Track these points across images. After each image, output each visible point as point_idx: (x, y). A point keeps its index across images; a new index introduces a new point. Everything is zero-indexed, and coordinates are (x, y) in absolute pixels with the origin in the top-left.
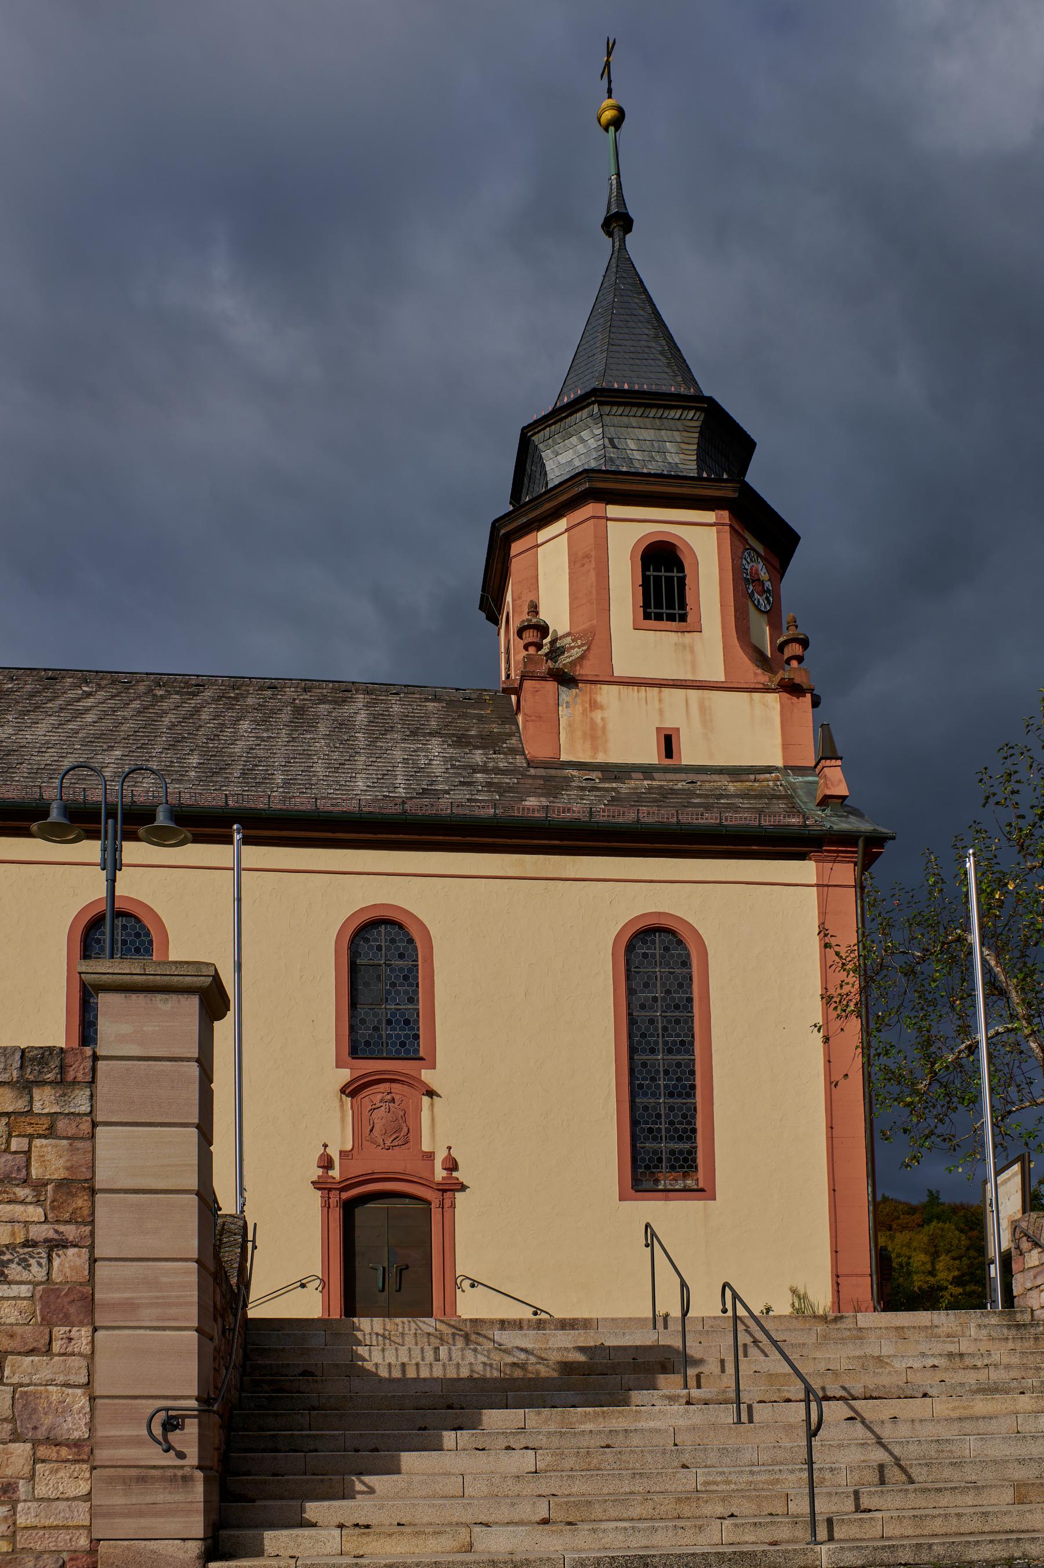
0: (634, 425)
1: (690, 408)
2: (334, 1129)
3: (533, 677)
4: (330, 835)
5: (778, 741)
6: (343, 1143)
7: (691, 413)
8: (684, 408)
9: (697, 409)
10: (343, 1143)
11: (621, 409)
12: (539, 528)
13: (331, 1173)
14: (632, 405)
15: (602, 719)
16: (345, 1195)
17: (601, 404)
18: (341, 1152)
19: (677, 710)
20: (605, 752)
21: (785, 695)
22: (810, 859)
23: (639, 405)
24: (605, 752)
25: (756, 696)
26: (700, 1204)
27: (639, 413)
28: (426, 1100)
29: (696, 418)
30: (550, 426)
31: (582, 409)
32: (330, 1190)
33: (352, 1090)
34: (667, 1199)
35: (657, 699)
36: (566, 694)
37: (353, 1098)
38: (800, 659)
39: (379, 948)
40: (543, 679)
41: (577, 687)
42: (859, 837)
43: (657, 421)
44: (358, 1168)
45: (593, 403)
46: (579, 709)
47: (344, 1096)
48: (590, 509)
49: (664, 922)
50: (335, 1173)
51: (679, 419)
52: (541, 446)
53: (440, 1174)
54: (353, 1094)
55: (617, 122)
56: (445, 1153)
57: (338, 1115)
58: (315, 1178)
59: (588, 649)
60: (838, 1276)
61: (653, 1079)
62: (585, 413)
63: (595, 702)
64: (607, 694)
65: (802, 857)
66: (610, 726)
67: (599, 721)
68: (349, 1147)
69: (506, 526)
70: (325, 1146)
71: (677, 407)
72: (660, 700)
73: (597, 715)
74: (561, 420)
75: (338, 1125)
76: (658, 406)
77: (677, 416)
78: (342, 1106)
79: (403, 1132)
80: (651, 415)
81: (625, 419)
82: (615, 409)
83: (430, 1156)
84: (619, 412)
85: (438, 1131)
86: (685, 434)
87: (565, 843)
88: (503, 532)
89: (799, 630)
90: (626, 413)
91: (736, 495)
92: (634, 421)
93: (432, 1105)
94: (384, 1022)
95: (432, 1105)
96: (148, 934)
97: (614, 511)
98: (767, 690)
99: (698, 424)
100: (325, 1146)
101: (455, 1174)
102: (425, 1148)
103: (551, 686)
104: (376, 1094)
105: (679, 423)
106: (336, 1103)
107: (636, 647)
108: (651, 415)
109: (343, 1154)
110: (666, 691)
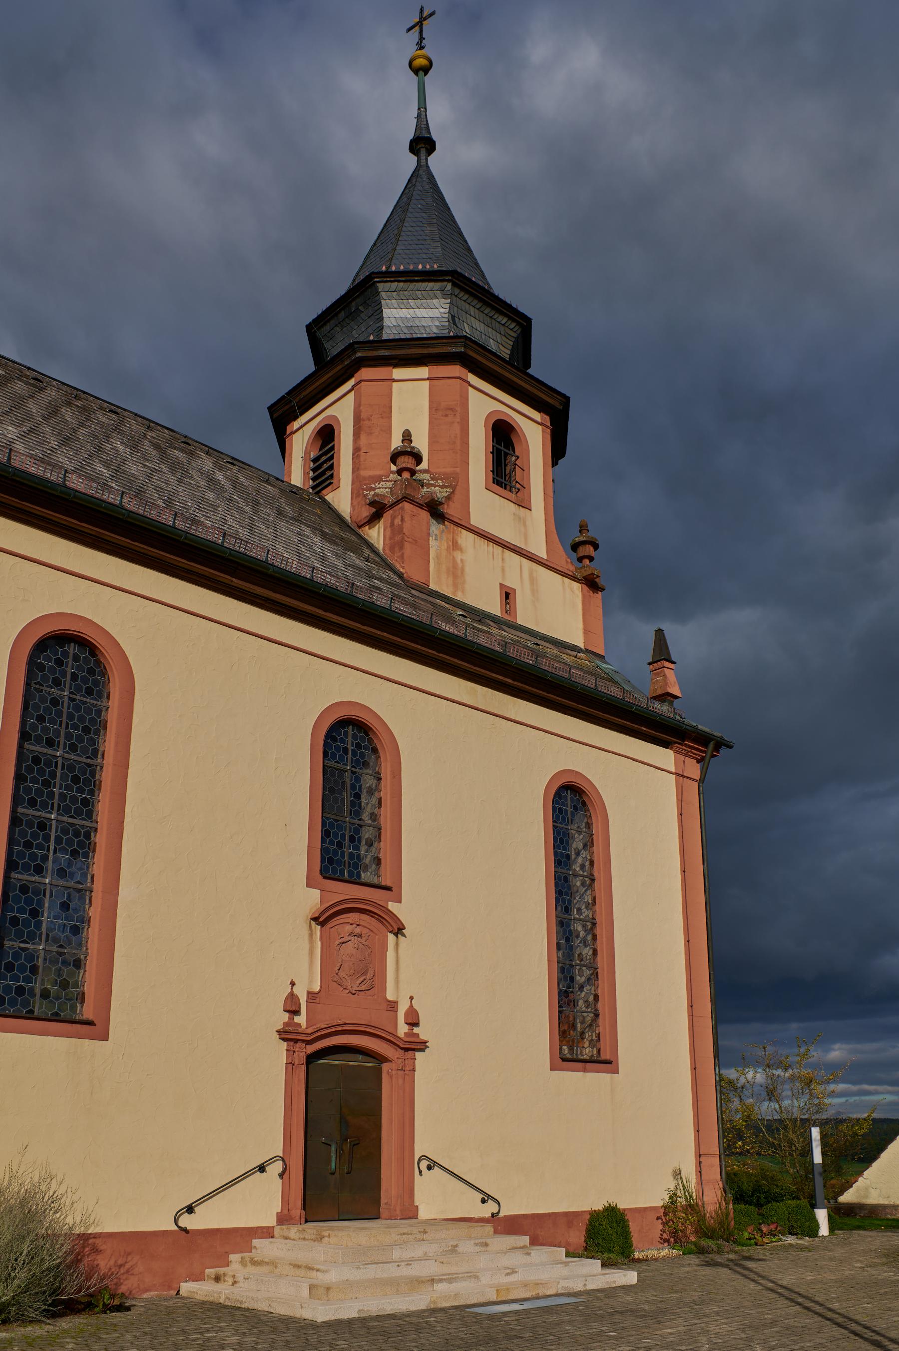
0: (472, 314)
1: (514, 320)
2: (301, 965)
3: (412, 501)
4: (321, 612)
5: (581, 625)
6: (311, 981)
7: (513, 325)
8: (510, 318)
9: (518, 323)
10: (311, 981)
11: (466, 297)
12: (396, 366)
13: (297, 1019)
14: (476, 297)
15: (462, 560)
16: (311, 1049)
17: (454, 285)
18: (309, 993)
19: (516, 572)
20: (463, 592)
21: (585, 587)
22: (671, 749)
23: (480, 300)
24: (463, 592)
25: (566, 580)
26: (607, 1076)
27: (478, 306)
28: (391, 937)
29: (515, 329)
30: (399, 281)
31: (429, 281)
32: (296, 1041)
33: (321, 919)
34: (585, 1070)
35: (500, 557)
36: (435, 528)
37: (322, 926)
38: (591, 559)
39: (346, 750)
40: (420, 506)
41: (444, 524)
42: (712, 740)
43: (488, 319)
44: (329, 1017)
45: (448, 281)
46: (444, 546)
47: (313, 923)
48: (456, 370)
49: (579, 782)
50: (301, 1020)
51: (503, 325)
52: (383, 294)
53: (402, 1029)
54: (322, 924)
55: (426, 70)
56: (407, 1006)
57: (307, 946)
58: (280, 1026)
59: (453, 492)
60: (700, 1156)
61: (46, 784)
62: (438, 285)
63: (457, 542)
64: (466, 539)
65: (665, 744)
66: (467, 570)
67: (459, 561)
68: (316, 988)
69: (365, 351)
70: (293, 984)
71: (505, 315)
72: (503, 559)
73: (458, 556)
74: (411, 281)
75: (306, 958)
76: (493, 308)
77: (503, 322)
78: (311, 935)
79: (369, 975)
80: (486, 312)
81: (467, 306)
82: (462, 294)
83: (393, 1006)
84: (464, 298)
85: (402, 976)
86: (504, 338)
87: (516, 683)
88: (359, 354)
89: (589, 534)
90: (469, 301)
91: (561, 408)
92: (472, 311)
93: (397, 945)
94: (347, 838)
95: (397, 945)
96: (104, 673)
97: (398, 373)
98: (574, 578)
99: (515, 335)
100: (293, 984)
101: (416, 1030)
102: (390, 996)
103: (425, 515)
104: (346, 925)
105: (502, 328)
106: (305, 932)
107: (485, 506)
108: (486, 312)
109: (311, 996)
110: (507, 553)
